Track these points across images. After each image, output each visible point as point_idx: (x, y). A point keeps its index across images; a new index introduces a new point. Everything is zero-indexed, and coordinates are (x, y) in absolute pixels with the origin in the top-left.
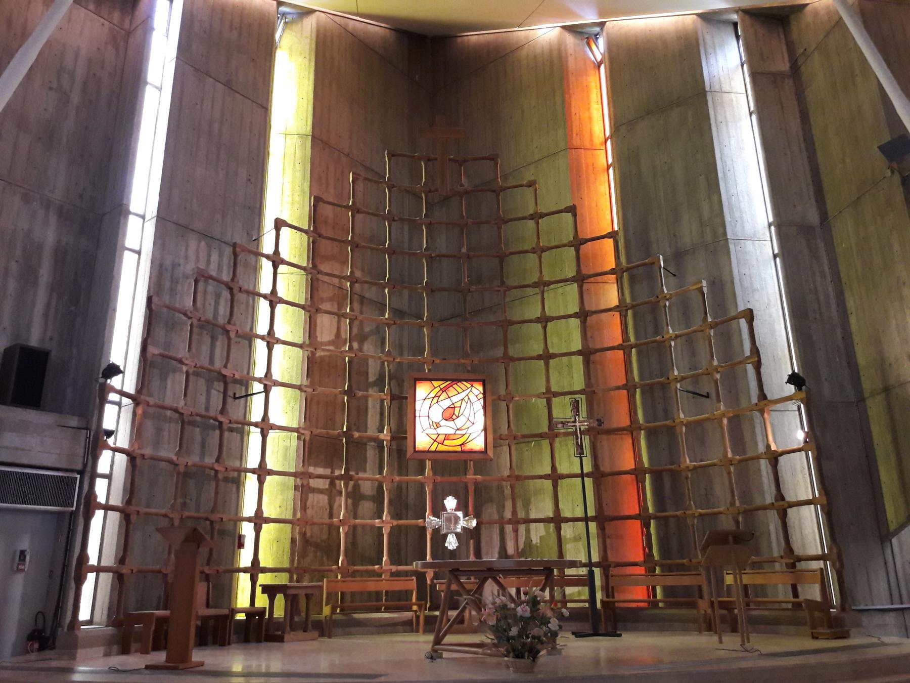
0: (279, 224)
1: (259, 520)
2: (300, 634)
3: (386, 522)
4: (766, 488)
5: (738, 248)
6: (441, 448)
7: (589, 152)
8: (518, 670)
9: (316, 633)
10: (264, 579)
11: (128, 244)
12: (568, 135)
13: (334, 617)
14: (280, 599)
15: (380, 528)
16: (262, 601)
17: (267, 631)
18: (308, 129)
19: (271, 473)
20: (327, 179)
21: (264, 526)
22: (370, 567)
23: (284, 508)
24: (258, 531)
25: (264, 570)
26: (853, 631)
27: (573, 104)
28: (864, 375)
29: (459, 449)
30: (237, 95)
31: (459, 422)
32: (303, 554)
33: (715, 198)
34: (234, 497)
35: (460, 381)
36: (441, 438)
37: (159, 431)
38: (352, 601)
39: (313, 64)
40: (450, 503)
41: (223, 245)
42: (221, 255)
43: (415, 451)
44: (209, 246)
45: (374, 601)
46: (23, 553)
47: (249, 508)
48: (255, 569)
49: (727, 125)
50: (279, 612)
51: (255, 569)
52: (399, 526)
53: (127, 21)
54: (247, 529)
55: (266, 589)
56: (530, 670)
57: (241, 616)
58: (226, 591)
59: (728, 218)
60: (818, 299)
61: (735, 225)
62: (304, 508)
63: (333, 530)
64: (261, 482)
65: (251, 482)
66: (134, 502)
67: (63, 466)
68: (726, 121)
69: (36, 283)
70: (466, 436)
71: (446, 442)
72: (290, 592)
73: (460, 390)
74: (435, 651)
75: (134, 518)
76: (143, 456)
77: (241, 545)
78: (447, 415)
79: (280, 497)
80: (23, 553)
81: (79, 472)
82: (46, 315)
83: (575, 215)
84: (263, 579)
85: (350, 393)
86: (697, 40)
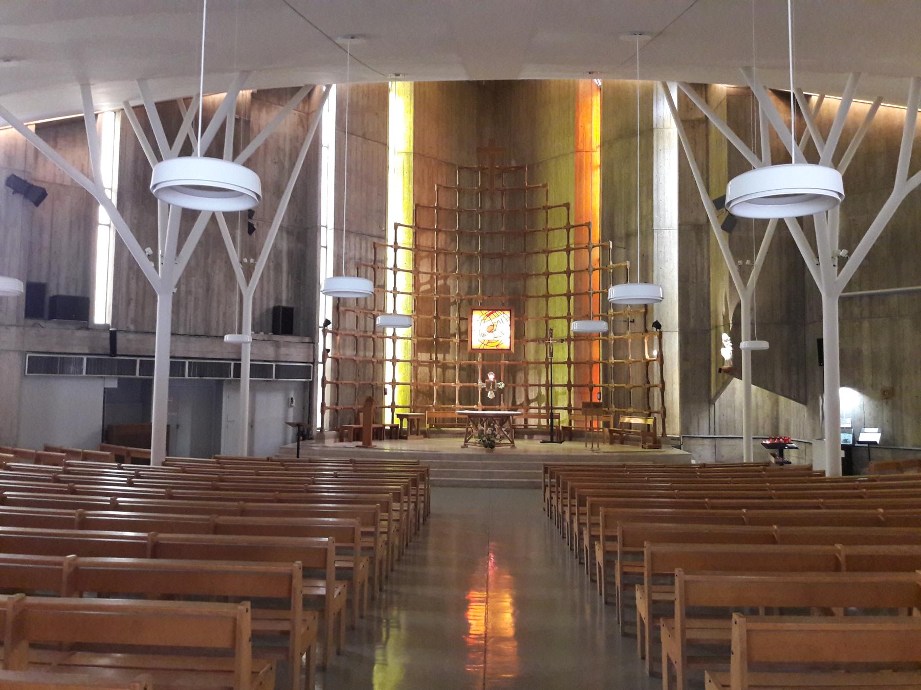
0: (396, 226)
1: (394, 384)
2: (415, 436)
3: (457, 385)
4: (655, 373)
5: (659, 235)
6: (486, 347)
7: (589, 153)
8: (487, 451)
9: (422, 436)
10: (398, 411)
11: (322, 244)
12: (576, 144)
13: (431, 429)
14: (405, 420)
15: (455, 387)
16: (397, 421)
17: (400, 434)
18: (411, 149)
19: (398, 361)
20: (423, 179)
21: (397, 386)
22: (449, 406)
23: (406, 374)
24: (394, 388)
25: (398, 407)
26: (663, 445)
27: (581, 117)
28: (834, 266)
29: (495, 348)
30: (370, 141)
31: (496, 334)
32: (417, 396)
33: (650, 202)
34: (381, 370)
35: (497, 310)
36: (486, 342)
37: (344, 341)
38: (439, 422)
39: (413, 101)
40: (491, 377)
41: (367, 237)
42: (366, 244)
43: (472, 349)
44: (361, 240)
45: (452, 422)
46: (292, 399)
47: (388, 378)
48: (393, 407)
49: (664, 152)
50: (405, 426)
51: (393, 407)
52: (464, 387)
53: (307, 108)
54: (389, 388)
55: (398, 416)
56: (492, 451)
57: (388, 428)
58: (380, 416)
59: (655, 216)
60: (697, 270)
61: (660, 220)
62: (416, 378)
63: (431, 388)
64: (394, 365)
65: (388, 366)
66: (340, 379)
67: (305, 361)
68: (664, 149)
69: (281, 272)
70: (499, 342)
71: (488, 344)
72: (409, 418)
73: (497, 316)
74: (465, 445)
75: (340, 386)
76: (342, 358)
77: (386, 393)
78: (490, 329)
79: (404, 368)
80: (292, 399)
81: (312, 363)
82: (287, 286)
83: (568, 209)
84: (398, 411)
85: (437, 317)
86: (652, 90)
